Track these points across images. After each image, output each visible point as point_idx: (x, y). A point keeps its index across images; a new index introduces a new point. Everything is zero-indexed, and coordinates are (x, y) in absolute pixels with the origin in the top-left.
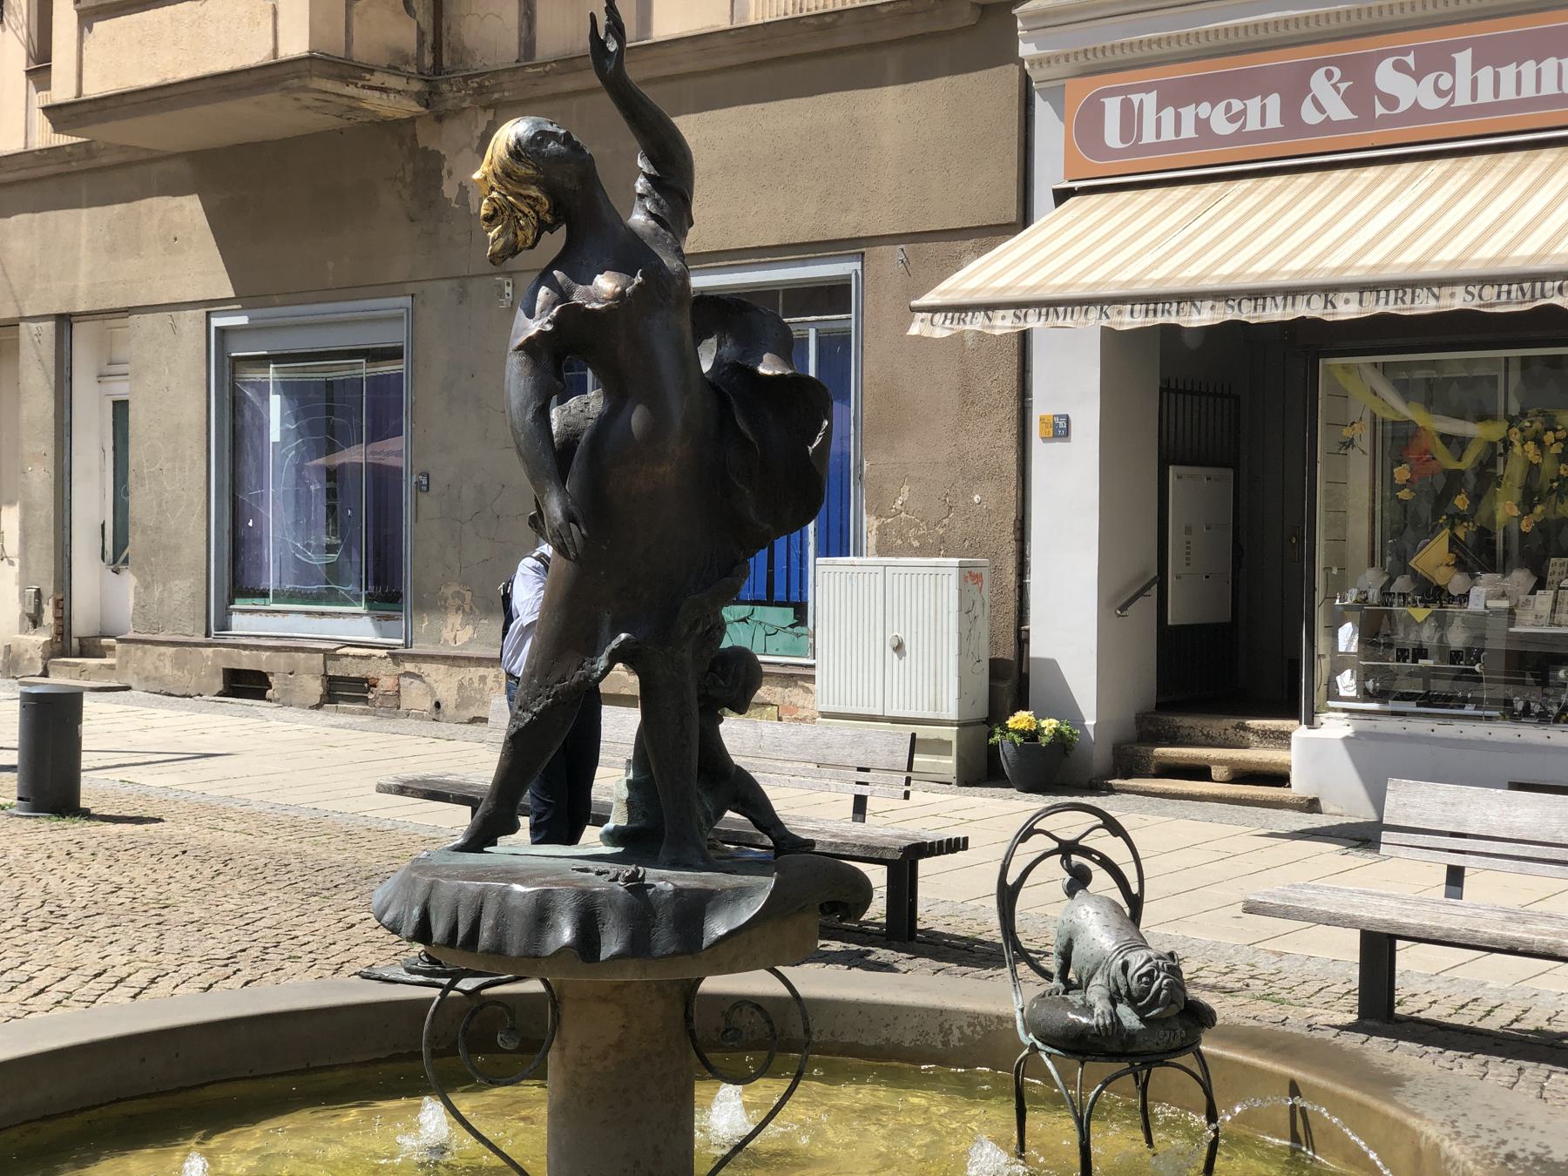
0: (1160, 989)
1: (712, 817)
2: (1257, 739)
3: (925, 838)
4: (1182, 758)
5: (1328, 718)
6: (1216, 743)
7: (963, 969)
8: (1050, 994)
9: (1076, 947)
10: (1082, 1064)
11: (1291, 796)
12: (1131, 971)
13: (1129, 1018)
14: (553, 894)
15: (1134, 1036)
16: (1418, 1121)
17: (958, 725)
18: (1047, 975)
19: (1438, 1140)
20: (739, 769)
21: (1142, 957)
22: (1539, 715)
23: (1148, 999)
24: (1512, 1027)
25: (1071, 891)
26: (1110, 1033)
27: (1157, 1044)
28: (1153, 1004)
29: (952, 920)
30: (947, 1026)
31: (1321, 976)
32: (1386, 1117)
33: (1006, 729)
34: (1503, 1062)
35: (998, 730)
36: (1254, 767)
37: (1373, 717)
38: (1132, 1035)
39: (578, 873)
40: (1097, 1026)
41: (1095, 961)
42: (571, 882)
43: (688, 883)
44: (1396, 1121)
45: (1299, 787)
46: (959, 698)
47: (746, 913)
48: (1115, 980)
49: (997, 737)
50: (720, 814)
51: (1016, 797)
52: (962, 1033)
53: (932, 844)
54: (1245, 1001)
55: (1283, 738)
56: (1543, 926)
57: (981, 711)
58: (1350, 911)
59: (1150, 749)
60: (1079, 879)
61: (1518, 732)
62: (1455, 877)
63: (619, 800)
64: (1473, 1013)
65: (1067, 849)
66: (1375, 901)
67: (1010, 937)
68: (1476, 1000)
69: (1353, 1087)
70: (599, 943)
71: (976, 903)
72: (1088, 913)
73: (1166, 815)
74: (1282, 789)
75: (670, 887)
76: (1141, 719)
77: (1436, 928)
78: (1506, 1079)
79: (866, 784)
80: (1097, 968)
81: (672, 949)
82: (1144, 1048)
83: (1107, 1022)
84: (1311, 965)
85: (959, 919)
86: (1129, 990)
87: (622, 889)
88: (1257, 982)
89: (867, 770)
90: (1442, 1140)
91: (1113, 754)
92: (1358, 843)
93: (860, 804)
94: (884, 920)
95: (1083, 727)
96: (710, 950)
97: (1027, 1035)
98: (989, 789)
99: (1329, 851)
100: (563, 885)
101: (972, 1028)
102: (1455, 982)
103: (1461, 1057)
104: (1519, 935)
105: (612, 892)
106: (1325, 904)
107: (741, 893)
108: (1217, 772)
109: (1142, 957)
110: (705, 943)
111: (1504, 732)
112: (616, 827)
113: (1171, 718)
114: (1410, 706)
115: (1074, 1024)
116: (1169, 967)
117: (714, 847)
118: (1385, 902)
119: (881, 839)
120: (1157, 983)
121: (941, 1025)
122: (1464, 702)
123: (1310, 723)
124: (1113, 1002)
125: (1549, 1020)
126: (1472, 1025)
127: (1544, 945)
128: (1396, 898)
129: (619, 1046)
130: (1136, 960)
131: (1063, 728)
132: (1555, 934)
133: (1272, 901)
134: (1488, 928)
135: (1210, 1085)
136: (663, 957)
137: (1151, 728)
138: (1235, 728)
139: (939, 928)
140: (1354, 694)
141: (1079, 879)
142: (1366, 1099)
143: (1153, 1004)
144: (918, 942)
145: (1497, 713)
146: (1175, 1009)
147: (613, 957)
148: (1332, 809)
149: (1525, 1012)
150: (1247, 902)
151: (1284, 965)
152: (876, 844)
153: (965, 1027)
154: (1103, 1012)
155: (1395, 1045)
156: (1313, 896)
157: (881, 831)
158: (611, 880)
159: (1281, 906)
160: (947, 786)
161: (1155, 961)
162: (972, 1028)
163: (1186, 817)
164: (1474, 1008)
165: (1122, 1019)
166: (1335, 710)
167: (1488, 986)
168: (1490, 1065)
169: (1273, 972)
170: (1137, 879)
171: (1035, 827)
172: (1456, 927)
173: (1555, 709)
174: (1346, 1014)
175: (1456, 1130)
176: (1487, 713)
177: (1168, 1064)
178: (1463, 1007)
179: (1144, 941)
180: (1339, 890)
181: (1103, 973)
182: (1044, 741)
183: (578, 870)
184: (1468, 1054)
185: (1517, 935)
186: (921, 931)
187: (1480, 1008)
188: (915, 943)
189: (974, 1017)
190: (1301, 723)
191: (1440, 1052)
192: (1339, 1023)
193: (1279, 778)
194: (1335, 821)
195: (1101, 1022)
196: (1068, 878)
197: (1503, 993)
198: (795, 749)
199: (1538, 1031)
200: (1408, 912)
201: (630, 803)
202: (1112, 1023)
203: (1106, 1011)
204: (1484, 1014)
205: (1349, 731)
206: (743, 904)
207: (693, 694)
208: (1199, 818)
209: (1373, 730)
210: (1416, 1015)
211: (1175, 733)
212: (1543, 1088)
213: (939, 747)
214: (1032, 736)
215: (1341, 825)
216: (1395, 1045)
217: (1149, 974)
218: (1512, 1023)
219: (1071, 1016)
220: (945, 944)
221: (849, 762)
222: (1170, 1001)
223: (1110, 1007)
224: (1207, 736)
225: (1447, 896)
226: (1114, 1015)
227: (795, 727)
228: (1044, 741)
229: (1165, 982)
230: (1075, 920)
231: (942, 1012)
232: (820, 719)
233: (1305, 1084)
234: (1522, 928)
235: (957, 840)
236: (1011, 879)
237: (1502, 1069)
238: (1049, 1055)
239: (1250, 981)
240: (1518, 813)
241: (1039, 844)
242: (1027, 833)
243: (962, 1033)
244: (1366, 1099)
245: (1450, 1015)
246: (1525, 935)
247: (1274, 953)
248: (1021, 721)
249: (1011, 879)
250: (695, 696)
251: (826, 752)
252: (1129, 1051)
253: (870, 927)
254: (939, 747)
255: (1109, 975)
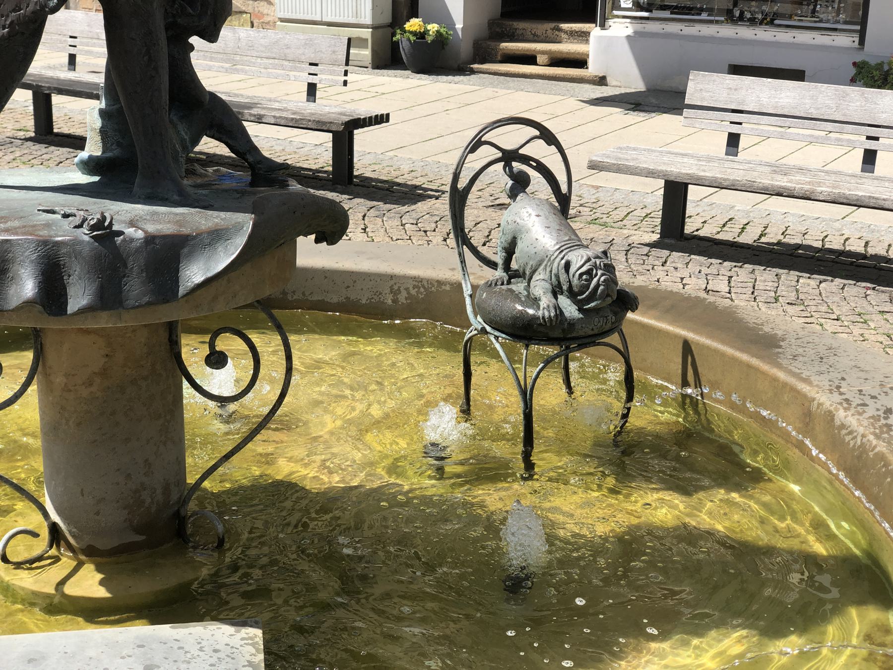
0: (598, 285)
1: (188, 144)
2: (566, 36)
3: (359, 115)
4: (518, 50)
5: (614, 22)
6: (540, 39)
7: (388, 206)
8: (496, 284)
9: (520, 247)
10: (527, 346)
11: (588, 75)
12: (572, 269)
13: (570, 310)
14: (12, 245)
15: (573, 324)
16: (808, 388)
17: (372, 28)
18: (493, 265)
19: (832, 408)
20: (213, 96)
21: (582, 257)
22: (750, 20)
23: (587, 293)
24: (761, 241)
25: (513, 194)
26: (554, 323)
27: (593, 329)
28: (592, 297)
29: (376, 167)
30: (396, 287)
31: (626, 204)
32: (775, 379)
33: (404, 31)
34: (764, 270)
35: (398, 31)
36: (564, 56)
37: (643, 21)
38: (572, 324)
39: (45, 214)
40: (543, 318)
41: (539, 259)
42: (31, 229)
43: (159, 227)
44: (785, 385)
45: (593, 69)
46: (373, 9)
47: (222, 259)
48: (557, 276)
49: (398, 36)
50: (196, 142)
51: (411, 77)
52: (408, 293)
53: (365, 119)
54: (582, 225)
55: (584, 36)
56: (798, 177)
57: (387, 18)
58: (663, 168)
59: (498, 44)
60: (520, 183)
61: (794, 35)
62: (733, 140)
63: (93, 129)
64: (733, 230)
65: (509, 157)
66: (679, 159)
67: (460, 234)
68: (730, 220)
69: (742, 350)
70: (66, 294)
71: (391, 154)
72: (530, 215)
73: (509, 89)
74: (582, 70)
75: (140, 234)
76: (492, 23)
77: (725, 180)
78: (771, 284)
79: (316, 75)
80: (540, 265)
81: (146, 299)
82: (581, 333)
83: (552, 315)
84: (617, 196)
85: (381, 166)
86: (570, 287)
87: (87, 238)
88: (586, 209)
89: (316, 65)
90: (837, 410)
91: (474, 47)
92: (633, 106)
93: (312, 90)
94: (331, 169)
95: (454, 29)
96: (185, 298)
97: (476, 317)
98: (393, 71)
99: (616, 114)
100: (24, 234)
101: (416, 290)
102: (714, 206)
103: (735, 266)
104: (785, 184)
105: (76, 242)
106: (645, 162)
107: (217, 236)
108: (540, 59)
109: (582, 257)
110: (182, 291)
111: (727, 31)
112: (90, 157)
113: (511, 23)
114: (666, 14)
115: (523, 314)
116: (605, 265)
117: (190, 173)
118: (685, 160)
119: (329, 115)
120: (595, 280)
121: (391, 287)
122: (700, 11)
123: (603, 26)
124: (555, 294)
125: (783, 234)
126: (735, 240)
127: (803, 192)
128: (692, 157)
129: (104, 373)
130: (577, 258)
131: (442, 30)
132: (809, 183)
133: (608, 161)
134: (762, 179)
135: (629, 355)
136: (134, 308)
137: (498, 30)
138: (553, 29)
139: (368, 174)
140: (630, 6)
141: (520, 183)
142: (755, 362)
143: (592, 297)
144: (355, 185)
145: (723, 19)
146: (609, 300)
147: (82, 311)
148: (614, 83)
149: (766, 228)
150: (591, 161)
151: (601, 195)
152: (324, 119)
153: (411, 289)
154: (548, 306)
155: (689, 258)
156: (635, 156)
157: (327, 109)
158: (76, 227)
159: (615, 164)
160: (365, 69)
161: (593, 260)
162: (416, 290)
163: (522, 90)
164: (732, 226)
165: (564, 310)
166: (618, 17)
167: (736, 208)
168: (756, 272)
169: (595, 201)
170: (566, 180)
171: (483, 139)
172: (739, 179)
173: (760, 16)
174: (651, 234)
175: (844, 397)
176: (717, 18)
177: (599, 344)
178: (724, 226)
179: (580, 240)
180: (652, 151)
181: (545, 269)
182: (429, 39)
183: (44, 211)
184: (740, 264)
185: (783, 184)
186: (357, 177)
187: (736, 226)
188: (352, 186)
189: (418, 282)
190: (596, 26)
191: (720, 263)
192: (648, 241)
193: (580, 62)
194: (617, 91)
195: (547, 314)
196: (510, 183)
197: (748, 213)
198: (264, 49)
199: (779, 243)
200: (703, 168)
201: (103, 132)
202: (556, 315)
203: (551, 305)
204: (740, 230)
205: (630, 31)
206: (220, 249)
207: (159, 22)
208: (531, 90)
209: (642, 30)
210: (695, 233)
211: (514, 33)
212: (797, 291)
213: (361, 43)
214: (421, 35)
215: (621, 94)
216: (689, 258)
217: (589, 272)
218: (761, 236)
219: (519, 308)
220: (373, 186)
221: (303, 58)
222: (606, 295)
223: (554, 300)
224: (534, 35)
225: (727, 154)
226: (557, 308)
227: (263, 33)
228: (429, 39)
229: (602, 279)
230: (518, 221)
231: (392, 277)
232: (279, 23)
233: (698, 344)
234: (785, 178)
235: (382, 115)
236: (462, 184)
237: (765, 275)
238: (497, 338)
239: (581, 209)
240: (782, 95)
241: (486, 153)
242: (476, 145)
243: (408, 293)
244: (755, 362)
245: (719, 233)
246: (789, 185)
247: (593, 186)
248: (414, 25)
249: (462, 184)
250: (162, 27)
251: (288, 51)
252: (569, 336)
253: (320, 175)
254: (361, 43)
255: (551, 271)
